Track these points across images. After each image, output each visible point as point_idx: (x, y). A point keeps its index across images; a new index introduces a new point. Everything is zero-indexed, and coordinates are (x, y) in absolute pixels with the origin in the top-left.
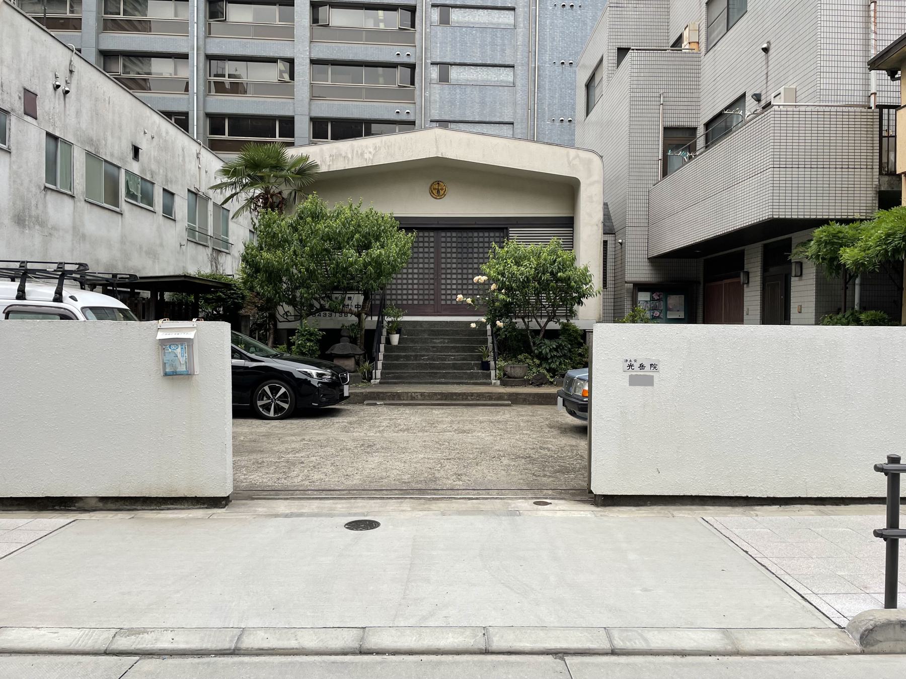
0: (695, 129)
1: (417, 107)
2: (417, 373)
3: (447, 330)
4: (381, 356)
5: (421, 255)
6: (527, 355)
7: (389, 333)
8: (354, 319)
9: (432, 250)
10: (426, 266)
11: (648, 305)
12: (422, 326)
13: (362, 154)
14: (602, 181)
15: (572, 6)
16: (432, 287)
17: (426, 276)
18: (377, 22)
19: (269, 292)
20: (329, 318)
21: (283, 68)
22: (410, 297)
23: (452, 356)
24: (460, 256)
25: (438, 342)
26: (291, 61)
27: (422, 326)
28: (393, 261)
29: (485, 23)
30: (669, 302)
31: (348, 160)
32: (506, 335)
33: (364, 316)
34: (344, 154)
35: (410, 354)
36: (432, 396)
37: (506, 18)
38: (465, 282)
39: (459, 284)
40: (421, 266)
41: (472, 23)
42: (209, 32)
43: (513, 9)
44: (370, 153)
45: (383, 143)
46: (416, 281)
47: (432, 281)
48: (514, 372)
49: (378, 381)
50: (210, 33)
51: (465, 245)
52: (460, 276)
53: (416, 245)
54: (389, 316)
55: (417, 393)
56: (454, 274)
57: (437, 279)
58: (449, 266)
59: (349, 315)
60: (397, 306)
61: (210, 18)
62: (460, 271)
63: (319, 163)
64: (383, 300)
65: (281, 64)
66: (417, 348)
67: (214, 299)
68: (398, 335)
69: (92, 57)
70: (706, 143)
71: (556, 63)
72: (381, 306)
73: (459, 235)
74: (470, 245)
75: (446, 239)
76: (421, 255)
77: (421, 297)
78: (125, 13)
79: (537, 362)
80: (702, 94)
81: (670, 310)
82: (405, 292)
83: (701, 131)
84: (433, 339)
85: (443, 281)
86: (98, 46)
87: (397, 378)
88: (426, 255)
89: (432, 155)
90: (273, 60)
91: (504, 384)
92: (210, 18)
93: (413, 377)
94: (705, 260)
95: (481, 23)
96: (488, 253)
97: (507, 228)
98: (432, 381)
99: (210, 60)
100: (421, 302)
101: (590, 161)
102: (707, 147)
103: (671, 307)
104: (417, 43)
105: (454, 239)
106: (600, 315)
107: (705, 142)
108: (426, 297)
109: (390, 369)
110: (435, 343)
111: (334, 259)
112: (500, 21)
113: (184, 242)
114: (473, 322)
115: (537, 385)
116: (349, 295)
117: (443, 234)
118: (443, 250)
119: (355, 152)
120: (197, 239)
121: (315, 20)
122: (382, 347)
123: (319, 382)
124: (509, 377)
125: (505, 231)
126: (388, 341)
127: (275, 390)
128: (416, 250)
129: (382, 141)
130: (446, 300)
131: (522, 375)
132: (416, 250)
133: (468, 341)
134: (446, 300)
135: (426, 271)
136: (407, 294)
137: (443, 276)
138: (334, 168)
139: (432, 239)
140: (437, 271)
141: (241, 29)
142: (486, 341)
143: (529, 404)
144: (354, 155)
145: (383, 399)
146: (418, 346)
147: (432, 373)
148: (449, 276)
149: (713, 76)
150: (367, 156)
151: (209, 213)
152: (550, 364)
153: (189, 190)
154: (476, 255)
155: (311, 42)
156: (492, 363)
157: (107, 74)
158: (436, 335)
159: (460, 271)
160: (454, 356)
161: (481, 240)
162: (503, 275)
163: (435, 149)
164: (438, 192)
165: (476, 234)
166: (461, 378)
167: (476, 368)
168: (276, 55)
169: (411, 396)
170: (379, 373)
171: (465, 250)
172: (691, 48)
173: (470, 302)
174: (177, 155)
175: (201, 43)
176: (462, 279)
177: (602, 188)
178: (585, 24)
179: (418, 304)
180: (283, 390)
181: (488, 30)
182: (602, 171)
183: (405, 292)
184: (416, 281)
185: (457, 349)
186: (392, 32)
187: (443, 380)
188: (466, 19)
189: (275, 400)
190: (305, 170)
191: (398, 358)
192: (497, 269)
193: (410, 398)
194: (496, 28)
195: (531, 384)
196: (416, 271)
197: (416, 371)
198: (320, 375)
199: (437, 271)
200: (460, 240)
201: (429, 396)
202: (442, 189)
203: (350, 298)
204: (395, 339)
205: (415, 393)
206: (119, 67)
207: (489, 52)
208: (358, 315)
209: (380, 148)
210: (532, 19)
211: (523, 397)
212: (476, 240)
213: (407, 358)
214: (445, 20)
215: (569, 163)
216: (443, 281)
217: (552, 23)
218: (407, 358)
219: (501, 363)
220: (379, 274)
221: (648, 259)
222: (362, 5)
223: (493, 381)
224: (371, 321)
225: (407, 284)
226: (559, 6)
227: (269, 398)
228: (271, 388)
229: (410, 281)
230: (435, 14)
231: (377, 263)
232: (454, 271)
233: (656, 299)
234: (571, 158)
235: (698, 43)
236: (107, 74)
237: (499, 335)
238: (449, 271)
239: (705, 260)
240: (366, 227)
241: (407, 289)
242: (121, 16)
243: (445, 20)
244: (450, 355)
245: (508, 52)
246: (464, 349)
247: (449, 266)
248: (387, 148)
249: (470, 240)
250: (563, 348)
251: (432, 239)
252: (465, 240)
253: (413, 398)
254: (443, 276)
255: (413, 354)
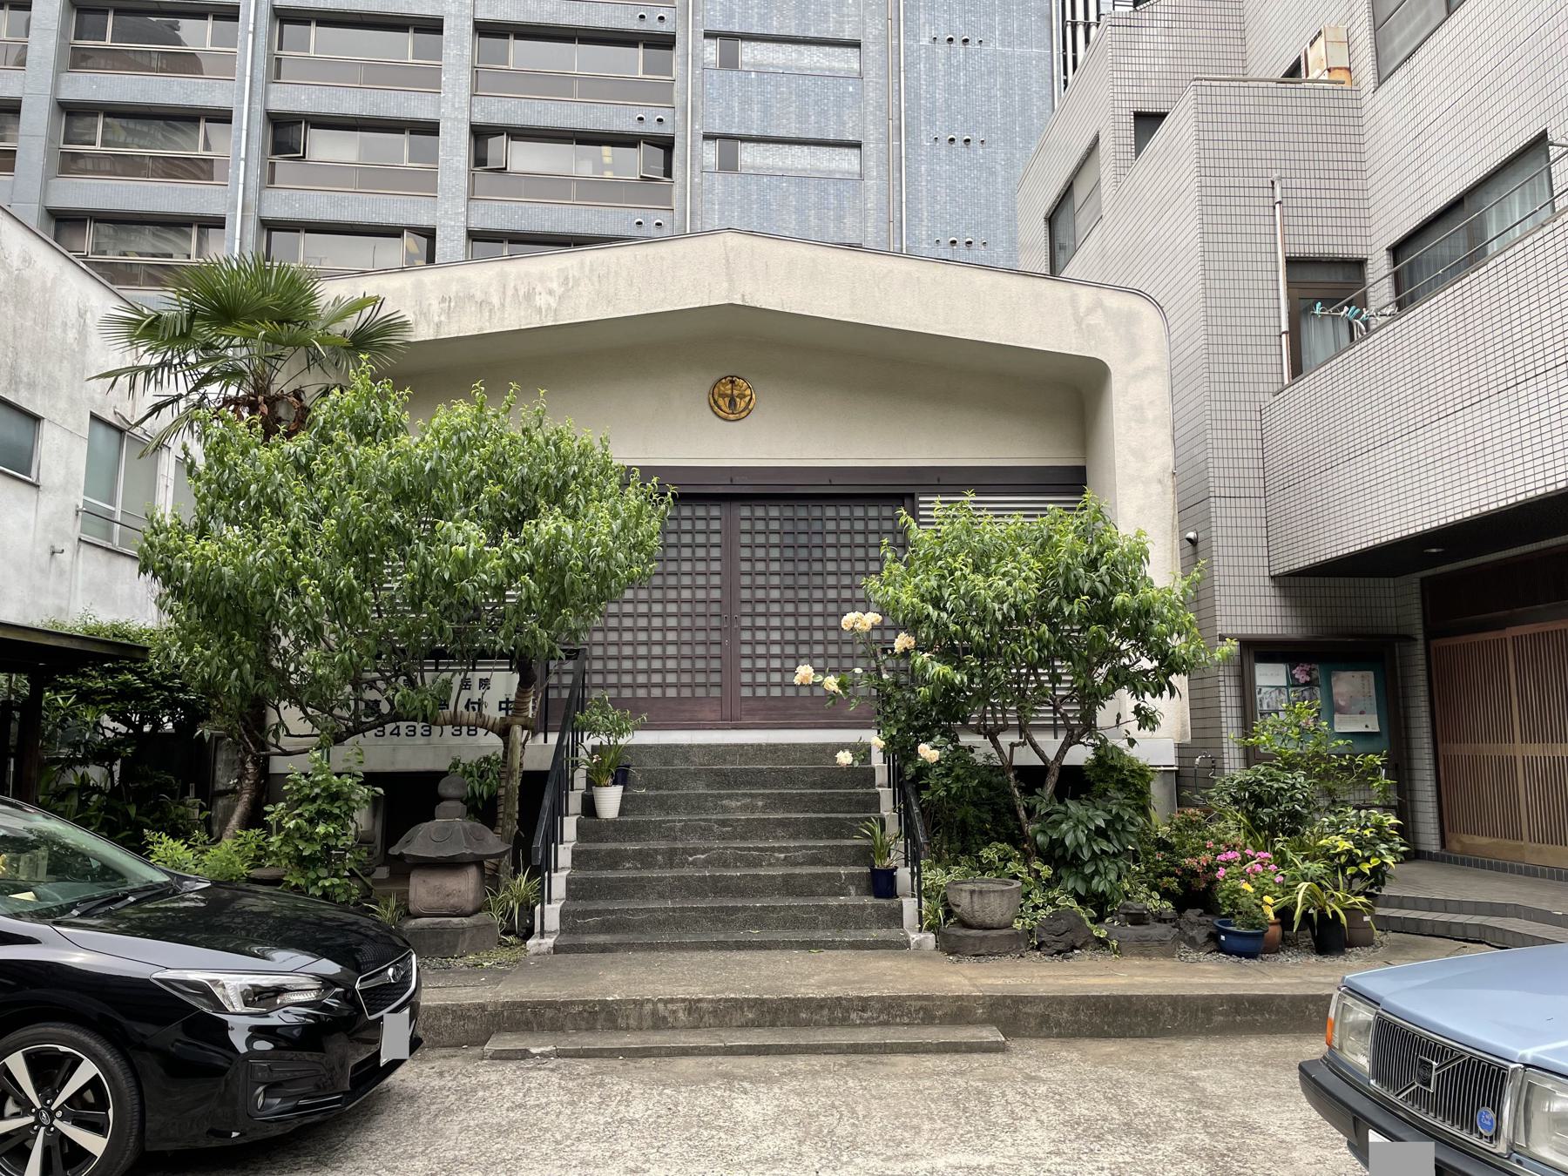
0: (1360, 264)
1: (676, 217)
2: (674, 910)
3: (760, 771)
4: (564, 855)
5: (686, 567)
6: (1005, 846)
7: (591, 783)
8: (491, 743)
9: (715, 553)
10: (701, 594)
11: (1284, 697)
12: (687, 759)
13: (529, 296)
14: (1166, 368)
15: (968, 140)
16: (715, 650)
17: (700, 622)
18: (602, 167)
19: (208, 664)
20: (423, 740)
21: (414, 249)
22: (657, 678)
23: (780, 850)
24: (789, 567)
25: (737, 807)
26: (429, 234)
27: (687, 759)
28: (601, 558)
29: (805, 170)
30: (1335, 690)
31: (490, 311)
32: (948, 788)
33: (519, 734)
34: (479, 296)
35: (654, 845)
36: (724, 1013)
37: (846, 161)
38: (804, 636)
39: (788, 643)
40: (686, 594)
41: (780, 169)
42: (270, 179)
43: (857, 145)
44: (551, 293)
45: (587, 270)
46: (671, 636)
47: (715, 636)
48: (983, 908)
49: (549, 942)
50: (272, 181)
51: (803, 539)
52: (790, 622)
53: (672, 526)
54: (594, 731)
55: (672, 1001)
56: (775, 615)
57: (729, 627)
58: (760, 594)
59: (481, 731)
60: (618, 703)
61: (274, 152)
62: (790, 608)
63: (410, 317)
64: (580, 685)
65: (411, 240)
66: (672, 829)
67: (108, 692)
68: (619, 788)
69: (33, 216)
70: (1398, 293)
71: (942, 242)
72: (568, 707)
73: (788, 512)
74: (817, 540)
75: (753, 525)
76: (686, 567)
77: (686, 678)
78: (105, 143)
79: (1046, 871)
80: (1370, 182)
81: (1340, 710)
82: (642, 665)
83: (1379, 267)
84: (721, 797)
85: (746, 636)
86: (44, 201)
87: (607, 928)
88: (701, 567)
89: (717, 296)
90: (394, 232)
91: (951, 947)
92: (274, 152)
93: (661, 925)
94: (1422, 580)
95: (797, 170)
96: (879, 546)
97: (912, 496)
98: (721, 937)
99: (270, 230)
100: (686, 693)
101: (1131, 318)
102: (1402, 305)
103: (1342, 703)
104: (675, 206)
105: (774, 525)
106: (1183, 725)
107: (1393, 289)
108: (700, 678)
109: (591, 898)
110: (725, 809)
111: (414, 556)
112: (833, 165)
113: (69, 546)
114: (842, 747)
115: (1059, 953)
116: (485, 675)
117: (745, 512)
118: (746, 553)
119: (510, 292)
120: (116, 540)
121: (479, 160)
122: (570, 826)
123: (258, 1032)
124: (966, 925)
125: (907, 502)
126: (589, 807)
127: (49, 1071)
128: (672, 539)
129: (582, 264)
130: (753, 685)
131: (1008, 916)
132: (672, 539)
133: (821, 803)
134: (753, 685)
135: (701, 608)
136: (649, 672)
137: (746, 622)
138: (451, 331)
139: (715, 525)
140: (729, 610)
141: (335, 174)
142: (873, 803)
143: (1059, 1035)
144: (508, 300)
145: (556, 1027)
146: (679, 819)
147: (721, 909)
148: (761, 622)
149: (1412, 125)
150: (541, 300)
151: (161, 482)
152: (1088, 879)
153: (94, 417)
154: (831, 567)
155: (470, 199)
156: (904, 875)
157: (70, 255)
158: (729, 786)
159: (790, 608)
160: (786, 849)
161: (845, 525)
162: (937, 603)
163: (725, 285)
164: (732, 403)
165: (830, 512)
166: (813, 925)
167: (852, 890)
168: (402, 221)
169: (654, 1013)
170: (551, 915)
171: (803, 553)
172: (1332, 78)
173: (835, 688)
174: (58, 323)
175: (252, 195)
176: (796, 629)
177: (1168, 384)
178: (993, 173)
179: (679, 699)
180: (87, 1071)
181: (812, 182)
182: (1166, 344)
183: (642, 665)
184: (671, 636)
185: (794, 829)
186: (628, 183)
187: (755, 934)
188: (770, 161)
189: (52, 1115)
190: (371, 336)
191: (614, 860)
192: (917, 587)
193: (648, 1022)
194: (828, 178)
195: (1038, 948)
196: (672, 608)
197: (670, 904)
198: (260, 997)
199: (729, 610)
200: (788, 526)
201: (715, 1012)
202: (742, 396)
203: (484, 683)
204: (610, 800)
205: (666, 1002)
206: (88, 240)
207: (813, 221)
208: (504, 732)
209: (577, 282)
210: (892, 165)
211: (1039, 1009)
212: (831, 526)
213: (645, 858)
214: (728, 164)
215: (1079, 323)
216: (746, 636)
217: (930, 172)
218: (645, 858)
219: (935, 876)
220: (558, 600)
221: (1272, 577)
222: (571, 135)
223: (915, 937)
224: (538, 751)
225: (649, 658)
226: (944, 141)
227: (25, 1106)
228: (37, 1064)
229: (657, 636)
230: (711, 153)
231: (549, 564)
232: (775, 608)
233: (1302, 681)
234: (1082, 310)
235: (1349, 69)
236: (70, 255)
237: (926, 787)
238: (761, 608)
239: (1422, 580)
240: (522, 460)
241: (649, 658)
242: (98, 146)
243: (728, 164)
244: (773, 849)
245: (848, 221)
246: (812, 829)
247: (760, 594)
248: (595, 279)
249: (817, 526)
250: (1124, 828)
251: (715, 525)
252: (802, 526)
253: (659, 1023)
254: (746, 622)
255: (663, 845)
